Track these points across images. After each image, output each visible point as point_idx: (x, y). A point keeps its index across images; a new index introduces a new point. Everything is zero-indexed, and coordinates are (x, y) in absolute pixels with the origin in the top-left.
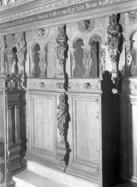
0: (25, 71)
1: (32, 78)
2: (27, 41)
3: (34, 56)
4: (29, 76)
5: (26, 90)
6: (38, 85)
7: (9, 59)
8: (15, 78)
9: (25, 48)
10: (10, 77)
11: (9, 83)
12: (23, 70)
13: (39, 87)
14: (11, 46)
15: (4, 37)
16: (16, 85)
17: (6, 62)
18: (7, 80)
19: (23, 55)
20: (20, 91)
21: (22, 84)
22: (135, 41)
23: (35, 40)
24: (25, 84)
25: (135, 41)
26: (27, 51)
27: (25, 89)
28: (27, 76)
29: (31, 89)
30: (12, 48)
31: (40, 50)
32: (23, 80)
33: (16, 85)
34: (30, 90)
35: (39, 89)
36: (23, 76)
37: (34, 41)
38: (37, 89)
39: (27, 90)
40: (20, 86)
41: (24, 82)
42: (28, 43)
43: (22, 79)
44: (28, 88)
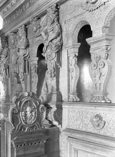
0: (58, 89)
1: (74, 102)
2: (63, 25)
3: (77, 54)
4: (67, 97)
5: (61, 130)
6: (87, 121)
7: (32, 68)
8: (36, 104)
9: (59, 38)
10: (24, 100)
11: (22, 114)
12: (55, 87)
13: (90, 125)
14: (36, 43)
15: (24, 29)
16: (39, 119)
17: (27, 74)
18: (17, 106)
19: (54, 55)
20: (47, 132)
21: (51, 116)
22: (59, 125)
23: (80, 17)
24: (58, 116)
25: (59, 125)
26: (62, 45)
27: (59, 126)
28: (63, 99)
29: (71, 127)
30: (37, 48)
31: (91, 36)
32: (54, 108)
33: (39, 119)
34: (68, 130)
35: (89, 130)
36: (54, 98)
37: (78, 20)
38: (84, 129)
39: (63, 130)
40: (46, 118)
41: (55, 112)
42: (64, 29)
43: (51, 106)
44: (65, 124)
